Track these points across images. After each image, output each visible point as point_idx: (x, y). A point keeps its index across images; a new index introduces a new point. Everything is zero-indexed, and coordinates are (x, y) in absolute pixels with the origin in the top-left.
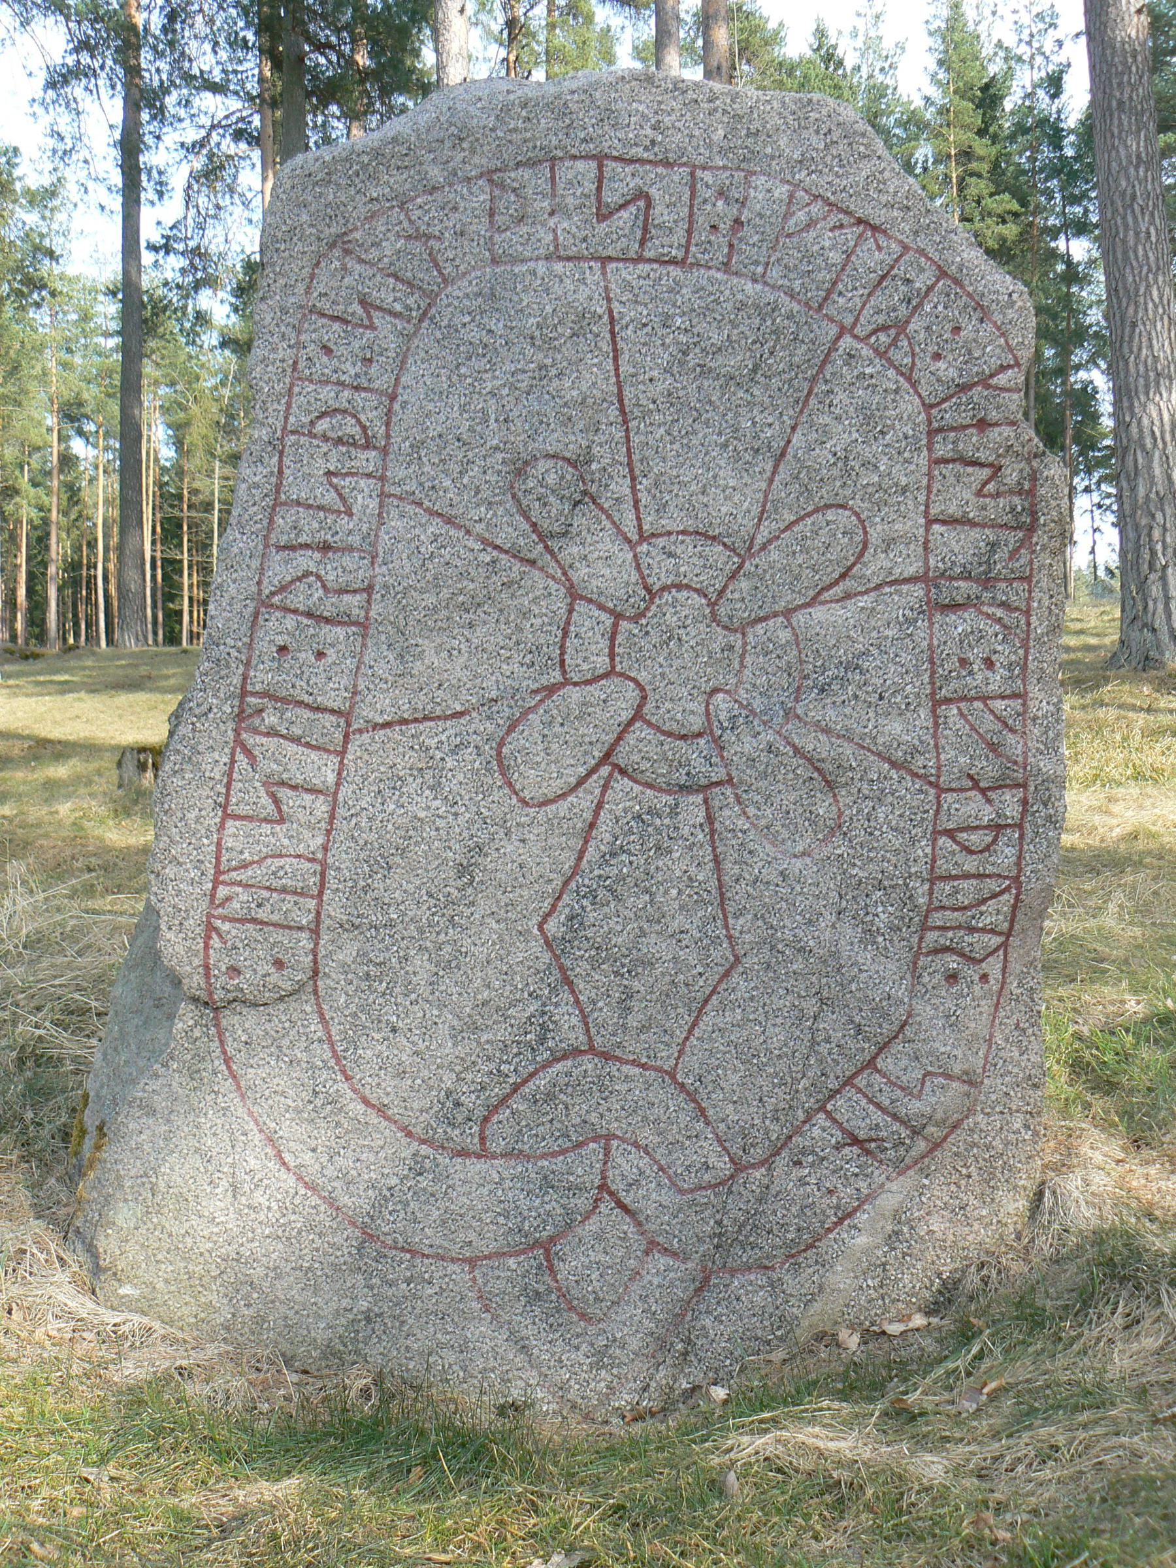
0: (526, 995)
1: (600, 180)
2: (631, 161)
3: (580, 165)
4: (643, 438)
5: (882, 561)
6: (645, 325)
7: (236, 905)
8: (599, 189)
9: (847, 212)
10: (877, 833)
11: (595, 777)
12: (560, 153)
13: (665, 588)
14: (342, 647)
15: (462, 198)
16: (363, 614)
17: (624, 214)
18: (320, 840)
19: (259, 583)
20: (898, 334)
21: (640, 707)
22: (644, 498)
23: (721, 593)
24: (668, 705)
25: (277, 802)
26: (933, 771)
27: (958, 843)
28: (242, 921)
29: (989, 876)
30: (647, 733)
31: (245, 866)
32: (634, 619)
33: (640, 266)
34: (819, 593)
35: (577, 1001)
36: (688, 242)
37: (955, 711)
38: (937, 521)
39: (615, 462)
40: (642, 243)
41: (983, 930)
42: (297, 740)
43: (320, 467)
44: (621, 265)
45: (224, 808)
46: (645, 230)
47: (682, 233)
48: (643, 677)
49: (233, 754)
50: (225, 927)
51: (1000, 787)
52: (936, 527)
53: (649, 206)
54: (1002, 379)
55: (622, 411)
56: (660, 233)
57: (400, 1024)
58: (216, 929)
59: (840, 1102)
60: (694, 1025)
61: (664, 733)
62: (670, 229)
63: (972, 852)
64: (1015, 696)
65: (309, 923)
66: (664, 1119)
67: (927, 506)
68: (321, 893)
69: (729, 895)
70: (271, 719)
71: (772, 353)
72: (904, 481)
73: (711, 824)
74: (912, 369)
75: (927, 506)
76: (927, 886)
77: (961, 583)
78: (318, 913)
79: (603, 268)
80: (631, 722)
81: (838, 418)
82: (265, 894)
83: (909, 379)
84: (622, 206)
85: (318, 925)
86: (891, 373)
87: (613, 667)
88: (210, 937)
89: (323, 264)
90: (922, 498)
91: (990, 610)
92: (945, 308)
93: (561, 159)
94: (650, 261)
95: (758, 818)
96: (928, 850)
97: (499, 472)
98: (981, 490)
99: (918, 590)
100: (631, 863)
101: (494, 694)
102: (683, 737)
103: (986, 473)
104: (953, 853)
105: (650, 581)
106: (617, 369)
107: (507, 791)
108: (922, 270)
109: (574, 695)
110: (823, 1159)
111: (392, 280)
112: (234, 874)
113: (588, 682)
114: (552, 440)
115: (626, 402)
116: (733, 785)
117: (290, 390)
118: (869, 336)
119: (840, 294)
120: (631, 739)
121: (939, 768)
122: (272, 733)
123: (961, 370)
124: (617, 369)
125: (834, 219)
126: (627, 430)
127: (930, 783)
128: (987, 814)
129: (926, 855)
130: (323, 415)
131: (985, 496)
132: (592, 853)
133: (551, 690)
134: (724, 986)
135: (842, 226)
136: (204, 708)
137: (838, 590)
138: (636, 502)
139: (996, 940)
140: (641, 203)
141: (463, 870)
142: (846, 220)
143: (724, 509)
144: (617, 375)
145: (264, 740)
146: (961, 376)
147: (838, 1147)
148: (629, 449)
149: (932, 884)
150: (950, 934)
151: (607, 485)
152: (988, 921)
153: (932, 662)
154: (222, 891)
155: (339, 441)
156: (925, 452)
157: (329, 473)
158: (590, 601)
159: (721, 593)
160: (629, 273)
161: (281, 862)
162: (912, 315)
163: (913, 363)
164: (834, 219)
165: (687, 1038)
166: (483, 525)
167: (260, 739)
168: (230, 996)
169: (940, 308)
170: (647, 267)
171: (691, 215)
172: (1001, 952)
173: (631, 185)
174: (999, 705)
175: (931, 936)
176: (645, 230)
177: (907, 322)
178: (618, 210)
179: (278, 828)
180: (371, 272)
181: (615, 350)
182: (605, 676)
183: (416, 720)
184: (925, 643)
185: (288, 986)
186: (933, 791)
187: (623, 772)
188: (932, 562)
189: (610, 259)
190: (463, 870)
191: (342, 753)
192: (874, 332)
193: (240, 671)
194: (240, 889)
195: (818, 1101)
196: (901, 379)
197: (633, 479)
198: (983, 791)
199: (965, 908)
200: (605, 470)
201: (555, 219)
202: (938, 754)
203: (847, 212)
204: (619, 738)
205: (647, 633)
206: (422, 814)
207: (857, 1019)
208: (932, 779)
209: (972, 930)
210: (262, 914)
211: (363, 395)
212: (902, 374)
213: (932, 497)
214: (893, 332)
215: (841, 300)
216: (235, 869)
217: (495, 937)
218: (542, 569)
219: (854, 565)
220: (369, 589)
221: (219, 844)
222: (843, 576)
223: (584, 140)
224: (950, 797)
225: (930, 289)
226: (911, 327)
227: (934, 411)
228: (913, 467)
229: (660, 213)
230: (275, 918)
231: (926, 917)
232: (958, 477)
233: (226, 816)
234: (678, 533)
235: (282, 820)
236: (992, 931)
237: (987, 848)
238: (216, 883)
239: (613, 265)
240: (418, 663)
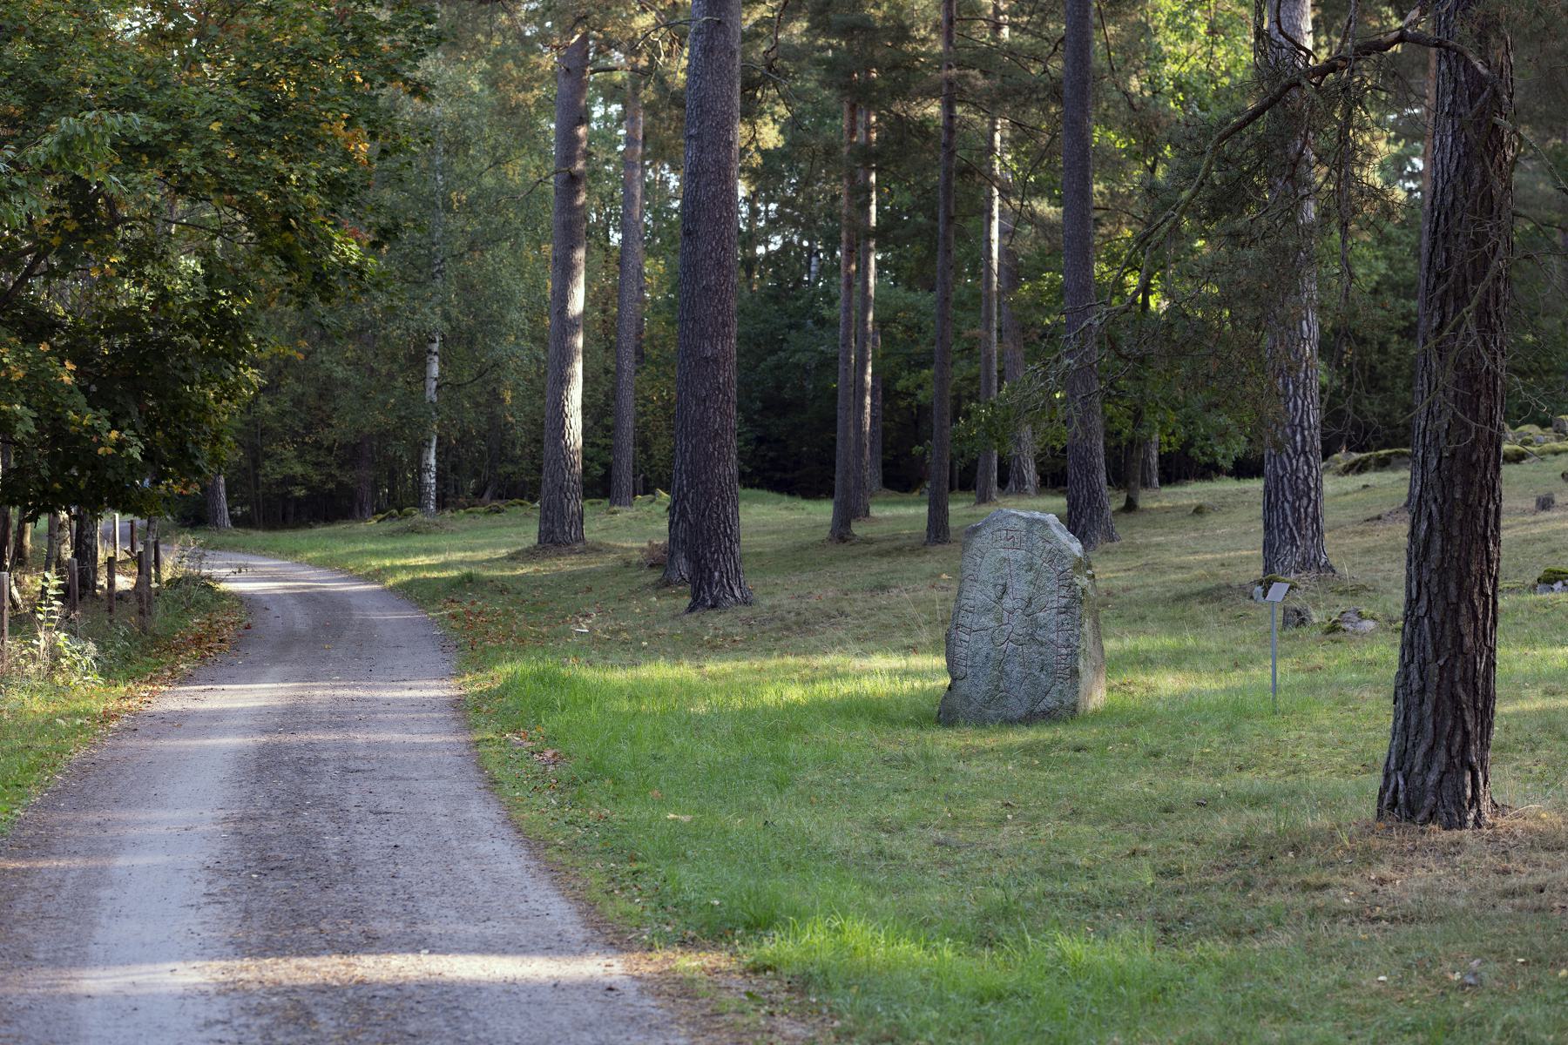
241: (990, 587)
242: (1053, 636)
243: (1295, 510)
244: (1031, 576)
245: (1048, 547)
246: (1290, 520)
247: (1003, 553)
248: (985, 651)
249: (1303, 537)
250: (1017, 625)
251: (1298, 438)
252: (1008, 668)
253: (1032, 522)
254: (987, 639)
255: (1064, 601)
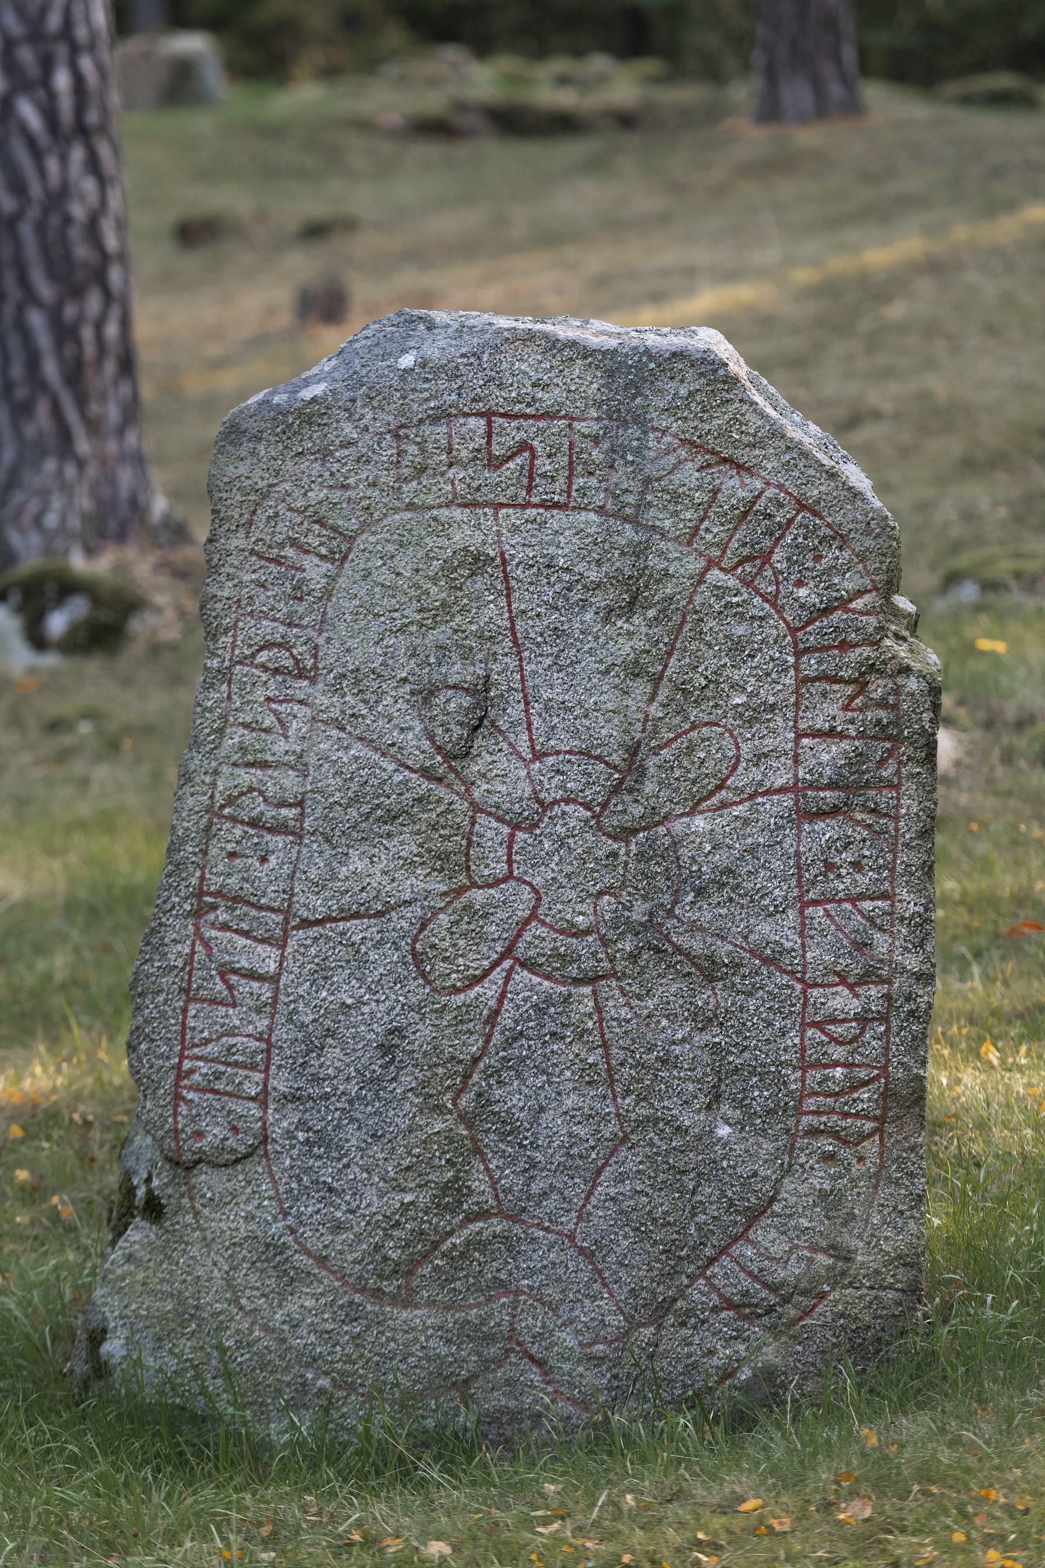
0: (443, 1162)
1: (489, 435)
2: (516, 417)
3: (472, 422)
4: (533, 667)
5: (756, 774)
6: (532, 566)
7: (197, 1077)
8: (489, 443)
9: (713, 453)
10: (749, 1024)
11: (499, 969)
12: (453, 411)
13: (556, 802)
14: (281, 854)
15: (374, 452)
16: (298, 825)
17: (511, 465)
18: (266, 1022)
19: (212, 797)
20: (763, 564)
21: (535, 908)
22: (536, 723)
23: (604, 806)
24: (559, 907)
25: (230, 988)
26: (799, 968)
27: (827, 1035)
28: (204, 1091)
29: (858, 1066)
30: (542, 931)
31: (207, 1042)
32: (530, 829)
33: (528, 511)
34: (698, 803)
35: (487, 1169)
36: (569, 487)
37: (821, 913)
38: (806, 736)
39: (510, 689)
40: (529, 490)
41: (857, 1115)
42: (246, 934)
43: (260, 694)
44: (511, 511)
45: (187, 991)
46: (531, 478)
47: (562, 480)
48: (538, 881)
49: (193, 945)
50: (191, 1096)
51: (866, 983)
52: (805, 741)
53: (533, 456)
54: (858, 604)
55: (515, 641)
56: (544, 482)
57: (335, 1184)
58: (183, 1099)
59: (716, 1269)
60: (590, 1193)
61: (556, 931)
62: (552, 477)
63: (841, 1044)
64: (884, 896)
65: (257, 1094)
66: (564, 1278)
67: (796, 722)
68: (267, 1068)
69: (617, 1077)
70: (223, 916)
71: (646, 587)
72: (771, 700)
73: (600, 1013)
74: (776, 596)
75: (796, 722)
76: (799, 1074)
77: (828, 794)
78: (265, 1085)
79: (496, 515)
80: (527, 921)
81: (710, 646)
82: (222, 1068)
83: (774, 605)
84: (510, 458)
85: (266, 1097)
86: (757, 600)
87: (511, 872)
88: (178, 1105)
89: (259, 512)
90: (790, 715)
91: (859, 816)
92: (805, 539)
93: (455, 416)
94: (536, 506)
95: (641, 1008)
96: (797, 1041)
97: (408, 701)
98: (849, 704)
99: (788, 801)
100: (529, 1046)
101: (407, 897)
102: (574, 935)
103: (850, 690)
104: (822, 1043)
105: (542, 795)
106: (509, 605)
107: (421, 981)
108: (781, 505)
109: (478, 896)
110: (703, 1322)
111: (317, 527)
112: (196, 1050)
113: (490, 886)
114: (457, 671)
115: (519, 635)
116: (618, 979)
117: (236, 623)
118: (735, 568)
119: (707, 530)
120: (527, 936)
121: (804, 966)
122: (225, 927)
123: (822, 595)
124: (509, 605)
125: (700, 460)
126: (521, 660)
127: (798, 980)
128: (854, 1006)
129: (795, 1045)
130: (262, 649)
131: (853, 710)
132: (497, 1038)
133: (460, 891)
134: (614, 1159)
135: (709, 466)
136: (169, 906)
137: (715, 800)
138: (529, 724)
139: (869, 1126)
140: (526, 454)
141: (385, 1049)
142: (713, 459)
143: (604, 732)
144: (510, 611)
145: (219, 934)
146: (821, 602)
147: (715, 1310)
148: (522, 676)
149: (805, 1072)
150: (824, 1119)
151: (504, 710)
152: (859, 1108)
153: (799, 868)
154: (187, 1065)
155: (277, 671)
156: (792, 672)
157: (269, 699)
158: (490, 814)
159: (604, 806)
160: (514, 516)
161: (232, 1041)
162: (775, 546)
163: (778, 591)
164: (700, 460)
165: (584, 1206)
166: (396, 749)
167: (214, 933)
168: (196, 1157)
169: (800, 540)
170: (534, 511)
171: (571, 463)
172: (877, 1138)
173: (517, 438)
174: (867, 905)
175: (806, 1120)
176: (531, 478)
177: (771, 552)
178: (506, 462)
179: (231, 1011)
180: (299, 520)
181: (508, 588)
182: (504, 880)
183: (343, 919)
184: (792, 850)
185: (242, 1149)
186: (799, 987)
187: (523, 965)
188: (801, 774)
189: (502, 505)
190: (385, 1049)
191: (283, 947)
192: (740, 563)
193: (198, 874)
194: (202, 1064)
195: (699, 1268)
196: (767, 606)
197: (527, 704)
198: (851, 987)
199: (837, 1094)
200: (502, 695)
201: (453, 471)
202: (805, 952)
203: (713, 453)
204: (519, 935)
205: (541, 842)
206: (349, 1001)
207: (729, 1194)
208: (799, 975)
209: (846, 1115)
210: (220, 1086)
211: (295, 630)
212: (767, 601)
213: (801, 714)
214: (758, 562)
215: (709, 537)
216: (197, 1046)
217: (414, 1109)
218: (448, 786)
219: (728, 777)
220: (300, 804)
221: (183, 1024)
222: (719, 787)
223: (474, 400)
224: (815, 992)
225: (790, 521)
226: (775, 557)
227: (800, 634)
228: (780, 687)
229: (544, 465)
230: (229, 1088)
231: (800, 1102)
232: (824, 695)
233: (189, 1000)
234: (566, 752)
235: (234, 1005)
236: (867, 1117)
237: (855, 1039)
238: (182, 1057)
239: (504, 511)
240: (344, 869)
241: (395, 702)
242: (783, 932)
243: (65, 333)
244: (628, 639)
245: (735, 488)
246: (51, 369)
247: (466, 532)
248: (378, 1014)
249: (94, 427)
250: (564, 885)
251: (62, 80)
252: (512, 1098)
253: (630, 375)
254: (384, 961)
255: (828, 755)
